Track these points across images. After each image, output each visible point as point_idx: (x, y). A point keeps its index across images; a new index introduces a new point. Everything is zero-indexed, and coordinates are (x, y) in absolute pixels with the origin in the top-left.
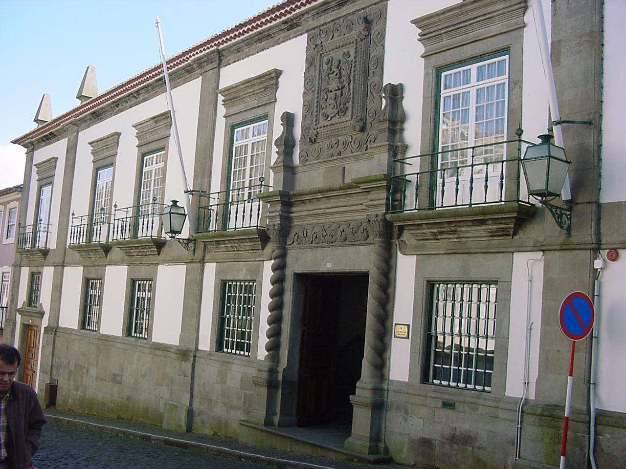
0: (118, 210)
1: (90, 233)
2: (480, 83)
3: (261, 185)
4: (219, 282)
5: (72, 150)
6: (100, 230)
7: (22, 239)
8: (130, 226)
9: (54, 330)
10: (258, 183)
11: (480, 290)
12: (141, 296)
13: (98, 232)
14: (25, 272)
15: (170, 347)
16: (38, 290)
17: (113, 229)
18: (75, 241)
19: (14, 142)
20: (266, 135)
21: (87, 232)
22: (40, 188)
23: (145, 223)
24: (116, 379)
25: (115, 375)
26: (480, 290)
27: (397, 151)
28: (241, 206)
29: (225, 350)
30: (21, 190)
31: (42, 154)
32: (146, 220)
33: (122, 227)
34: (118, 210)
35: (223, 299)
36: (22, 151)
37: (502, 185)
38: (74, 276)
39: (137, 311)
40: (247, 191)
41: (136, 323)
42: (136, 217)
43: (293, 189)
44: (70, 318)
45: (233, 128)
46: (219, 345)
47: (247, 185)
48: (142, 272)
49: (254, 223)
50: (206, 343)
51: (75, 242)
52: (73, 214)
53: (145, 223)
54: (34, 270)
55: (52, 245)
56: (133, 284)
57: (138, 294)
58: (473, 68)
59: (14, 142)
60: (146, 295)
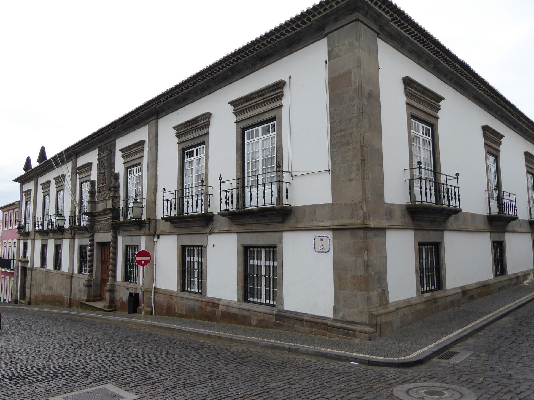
2: (264, 136)
3: (202, 186)
4: (242, 249)
5: (154, 137)
6: (164, 210)
7: (19, 228)
9: (32, 269)
11: (58, 248)
12: (195, 258)
13: (165, 208)
14: (22, 242)
15: (330, 318)
16: (60, 253)
18: (167, 214)
19: (14, 181)
20: (275, 133)
22: (58, 192)
23: (190, 203)
24: (51, 288)
25: (50, 287)
26: (58, 248)
27: (116, 198)
29: (186, 289)
30: (20, 202)
31: (26, 187)
32: (190, 200)
33: (227, 198)
36: (18, 184)
38: (38, 244)
39: (191, 271)
41: (188, 280)
42: (181, 199)
43: (95, 210)
44: (37, 263)
45: (128, 168)
46: (80, 271)
47: (260, 172)
49: (199, 209)
50: (76, 271)
53: (190, 203)
54: (25, 241)
55: (30, 230)
56: (185, 251)
58: (260, 128)
59: (14, 181)
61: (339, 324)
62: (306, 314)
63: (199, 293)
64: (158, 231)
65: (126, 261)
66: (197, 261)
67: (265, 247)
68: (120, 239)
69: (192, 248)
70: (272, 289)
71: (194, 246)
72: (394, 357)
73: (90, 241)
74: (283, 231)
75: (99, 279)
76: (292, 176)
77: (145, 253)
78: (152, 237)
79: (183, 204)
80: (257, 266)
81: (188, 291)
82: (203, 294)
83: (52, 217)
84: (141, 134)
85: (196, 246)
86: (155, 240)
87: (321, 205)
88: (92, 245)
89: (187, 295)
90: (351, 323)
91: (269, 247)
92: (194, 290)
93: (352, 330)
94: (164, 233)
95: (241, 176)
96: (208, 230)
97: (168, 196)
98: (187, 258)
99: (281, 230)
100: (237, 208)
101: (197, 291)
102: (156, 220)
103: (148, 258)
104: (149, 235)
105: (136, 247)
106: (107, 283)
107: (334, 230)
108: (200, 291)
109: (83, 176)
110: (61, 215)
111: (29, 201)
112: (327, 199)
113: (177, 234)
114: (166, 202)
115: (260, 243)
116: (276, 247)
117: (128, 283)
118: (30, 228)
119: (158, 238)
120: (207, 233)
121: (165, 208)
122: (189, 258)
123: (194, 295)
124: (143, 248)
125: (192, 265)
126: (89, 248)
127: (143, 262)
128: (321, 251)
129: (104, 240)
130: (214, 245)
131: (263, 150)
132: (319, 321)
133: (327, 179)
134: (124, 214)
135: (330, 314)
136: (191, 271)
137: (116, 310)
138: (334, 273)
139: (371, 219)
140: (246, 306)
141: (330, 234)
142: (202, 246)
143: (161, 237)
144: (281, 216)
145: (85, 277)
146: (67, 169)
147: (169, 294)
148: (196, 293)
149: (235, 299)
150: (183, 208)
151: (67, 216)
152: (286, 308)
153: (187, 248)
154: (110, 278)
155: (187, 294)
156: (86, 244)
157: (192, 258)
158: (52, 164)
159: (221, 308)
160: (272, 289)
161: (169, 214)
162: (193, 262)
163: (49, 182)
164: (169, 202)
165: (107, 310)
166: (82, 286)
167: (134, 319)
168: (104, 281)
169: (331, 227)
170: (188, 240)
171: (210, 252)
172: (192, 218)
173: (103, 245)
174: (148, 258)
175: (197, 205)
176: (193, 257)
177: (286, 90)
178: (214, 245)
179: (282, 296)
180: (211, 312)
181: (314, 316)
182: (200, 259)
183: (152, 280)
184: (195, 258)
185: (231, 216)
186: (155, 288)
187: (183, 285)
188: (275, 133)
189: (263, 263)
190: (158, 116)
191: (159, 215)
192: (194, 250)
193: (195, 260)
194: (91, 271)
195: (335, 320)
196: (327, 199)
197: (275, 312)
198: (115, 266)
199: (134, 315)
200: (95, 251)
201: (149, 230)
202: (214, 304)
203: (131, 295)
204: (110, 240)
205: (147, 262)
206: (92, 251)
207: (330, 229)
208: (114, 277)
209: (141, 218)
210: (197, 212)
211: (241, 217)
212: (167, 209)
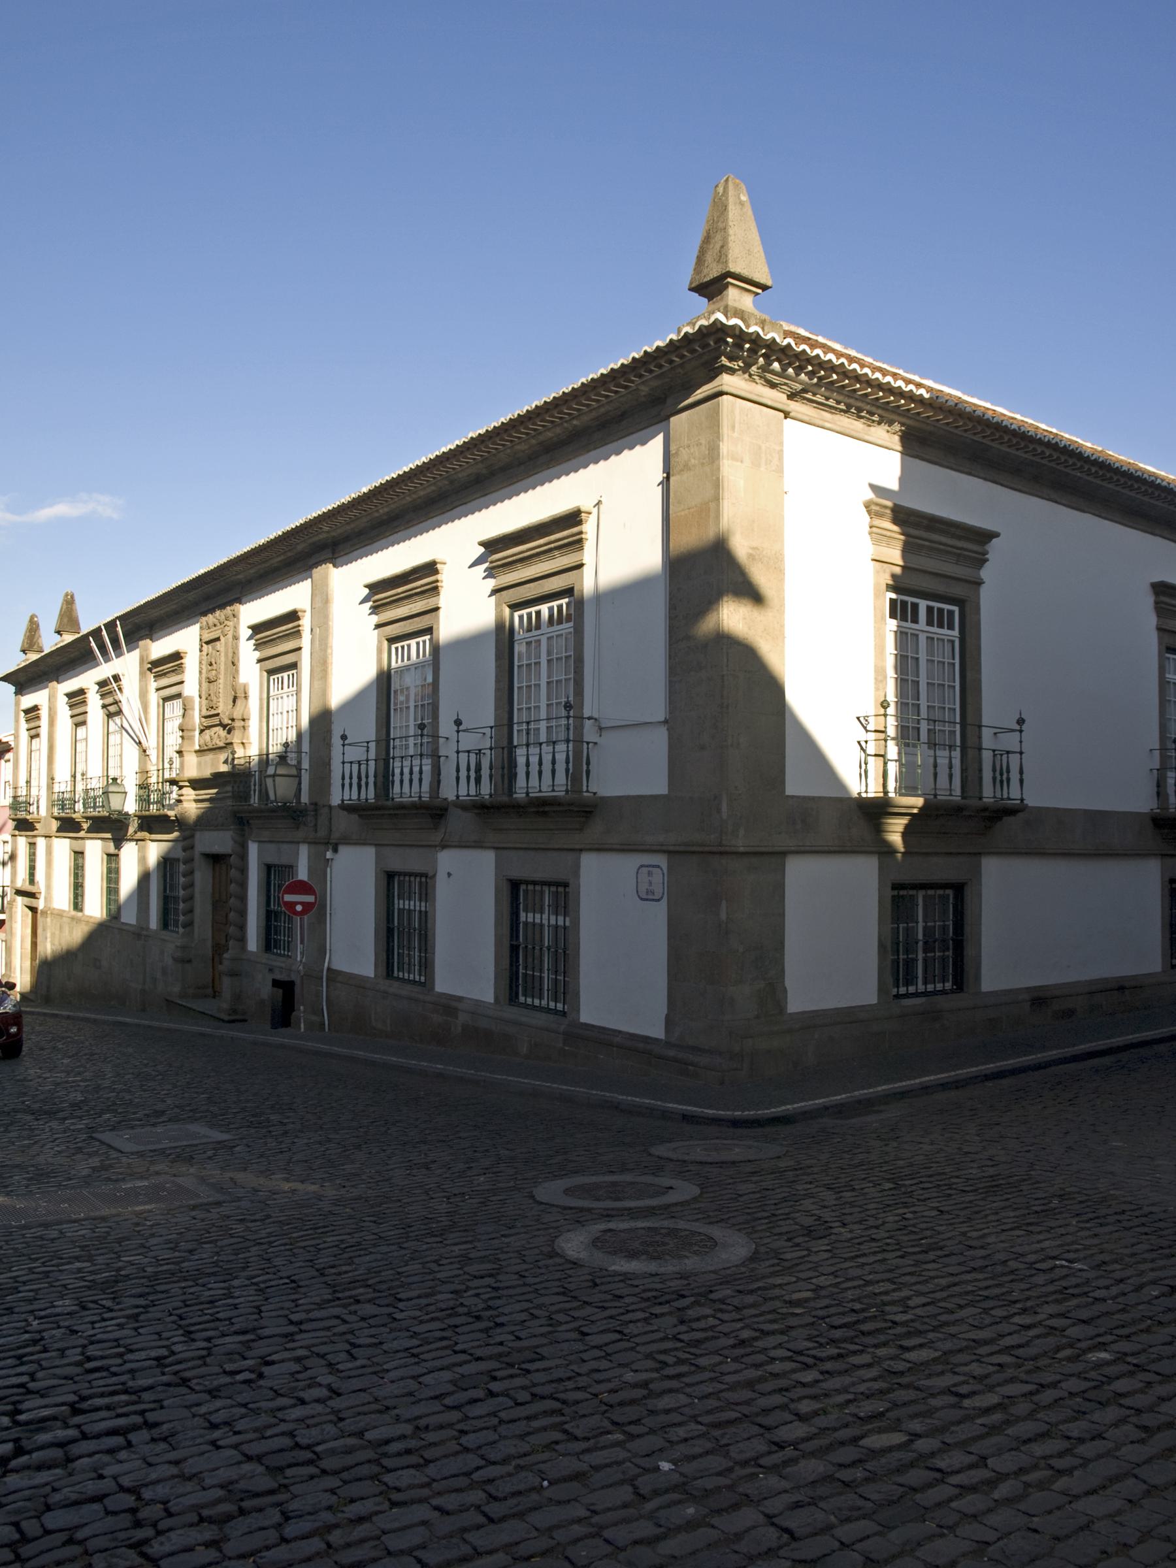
0: (349, 745)
1: (385, 779)
8: (491, 769)
10: (564, 713)
12: (545, 916)
13: (347, 781)
17: (550, 766)
21: (375, 777)
23: (406, 771)
28: (407, 763)
29: (395, 974)
31: (28, 701)
34: (349, 745)
35: (959, 946)
37: (588, 763)
39: (404, 934)
40: (543, 726)
46: (165, 923)
47: (543, 715)
48: (405, 861)
50: (154, 923)
51: (346, 797)
52: (344, 737)
53: (406, 771)
56: (391, 881)
57: (398, 904)
60: (414, 905)
61: (671, 1053)
62: (620, 1032)
63: (556, 1012)
64: (335, 835)
65: (268, 903)
66: (553, 922)
67: (549, 884)
68: (253, 849)
69: (538, 888)
70: (561, 978)
71: (410, 874)
72: (734, 1110)
73: (184, 850)
74: (581, 850)
75: (209, 944)
76: (601, 729)
77: (303, 888)
78: (322, 848)
79: (512, 764)
80: (420, 912)
81: (398, 979)
82: (427, 984)
83: (94, 784)
84: (292, 596)
85: (416, 875)
86: (329, 855)
87: (651, 796)
88: (190, 860)
89: (394, 988)
90: (696, 1049)
91: (557, 884)
92: (544, 1003)
93: (692, 1064)
94: (347, 840)
95: (384, 737)
96: (437, 837)
97: (469, 741)
98: (396, 901)
99: (577, 847)
100: (359, 799)
101: (552, 1005)
102: (330, 807)
103: (310, 899)
104: (315, 843)
105: (290, 868)
106: (225, 956)
107: (669, 852)
108: (560, 1006)
109: (165, 681)
110: (115, 780)
111: (37, 736)
112: (658, 786)
113: (376, 845)
114: (347, 766)
115: (538, 876)
116: (566, 885)
117: (272, 957)
118: (42, 810)
119: (335, 851)
120: (436, 846)
121: (347, 781)
122: (530, 915)
123: (543, 1016)
124: (303, 874)
125: (537, 937)
126: (182, 867)
127: (299, 908)
128: (648, 897)
129: (216, 849)
130: (449, 875)
131: (549, 661)
132: (641, 1045)
133: (661, 737)
134: (380, 779)
135: (656, 1030)
136: (404, 934)
137: (245, 1021)
138: (669, 945)
139: (742, 832)
140: (511, 1013)
141: (661, 860)
142: (566, 885)
143: (341, 848)
144: (574, 815)
145: (174, 941)
146: (127, 665)
147: (355, 982)
148: (548, 1010)
149: (489, 997)
150: (513, 776)
151: (131, 785)
152: (585, 1018)
153: (523, 887)
154: (231, 943)
155: (396, 984)
156: (176, 856)
157: (412, 903)
158: (91, 651)
159: (462, 1018)
160: (561, 978)
161: (355, 796)
162: (542, 925)
163: (81, 692)
164: (355, 767)
165: (226, 1018)
166: (169, 961)
167: (281, 1037)
168: (219, 949)
169: (664, 848)
170: (399, 861)
171: (443, 890)
172: (541, 807)
173: (216, 859)
174: (310, 899)
175: (540, 773)
176: (542, 913)
177: (588, 528)
178: (449, 875)
179: (578, 993)
180: (446, 1026)
181: (633, 1037)
182: (423, 904)
183: (322, 951)
184: (545, 916)
185: (482, 809)
186: (329, 969)
187: (388, 963)
188: (571, 624)
189: (547, 918)
190: (333, 553)
191: (335, 801)
192: (542, 892)
193: (545, 922)
194: (189, 925)
195: (668, 1044)
196: (658, 786)
197: (562, 1028)
198: (243, 913)
199: (283, 1030)
200: (198, 876)
201: (316, 831)
202: (449, 1005)
203: (276, 983)
204: (230, 851)
205: (307, 907)
206: (190, 873)
207: (664, 852)
208: (242, 940)
209: (299, 802)
210: (468, 795)
211: (502, 813)
212: (468, 777)
